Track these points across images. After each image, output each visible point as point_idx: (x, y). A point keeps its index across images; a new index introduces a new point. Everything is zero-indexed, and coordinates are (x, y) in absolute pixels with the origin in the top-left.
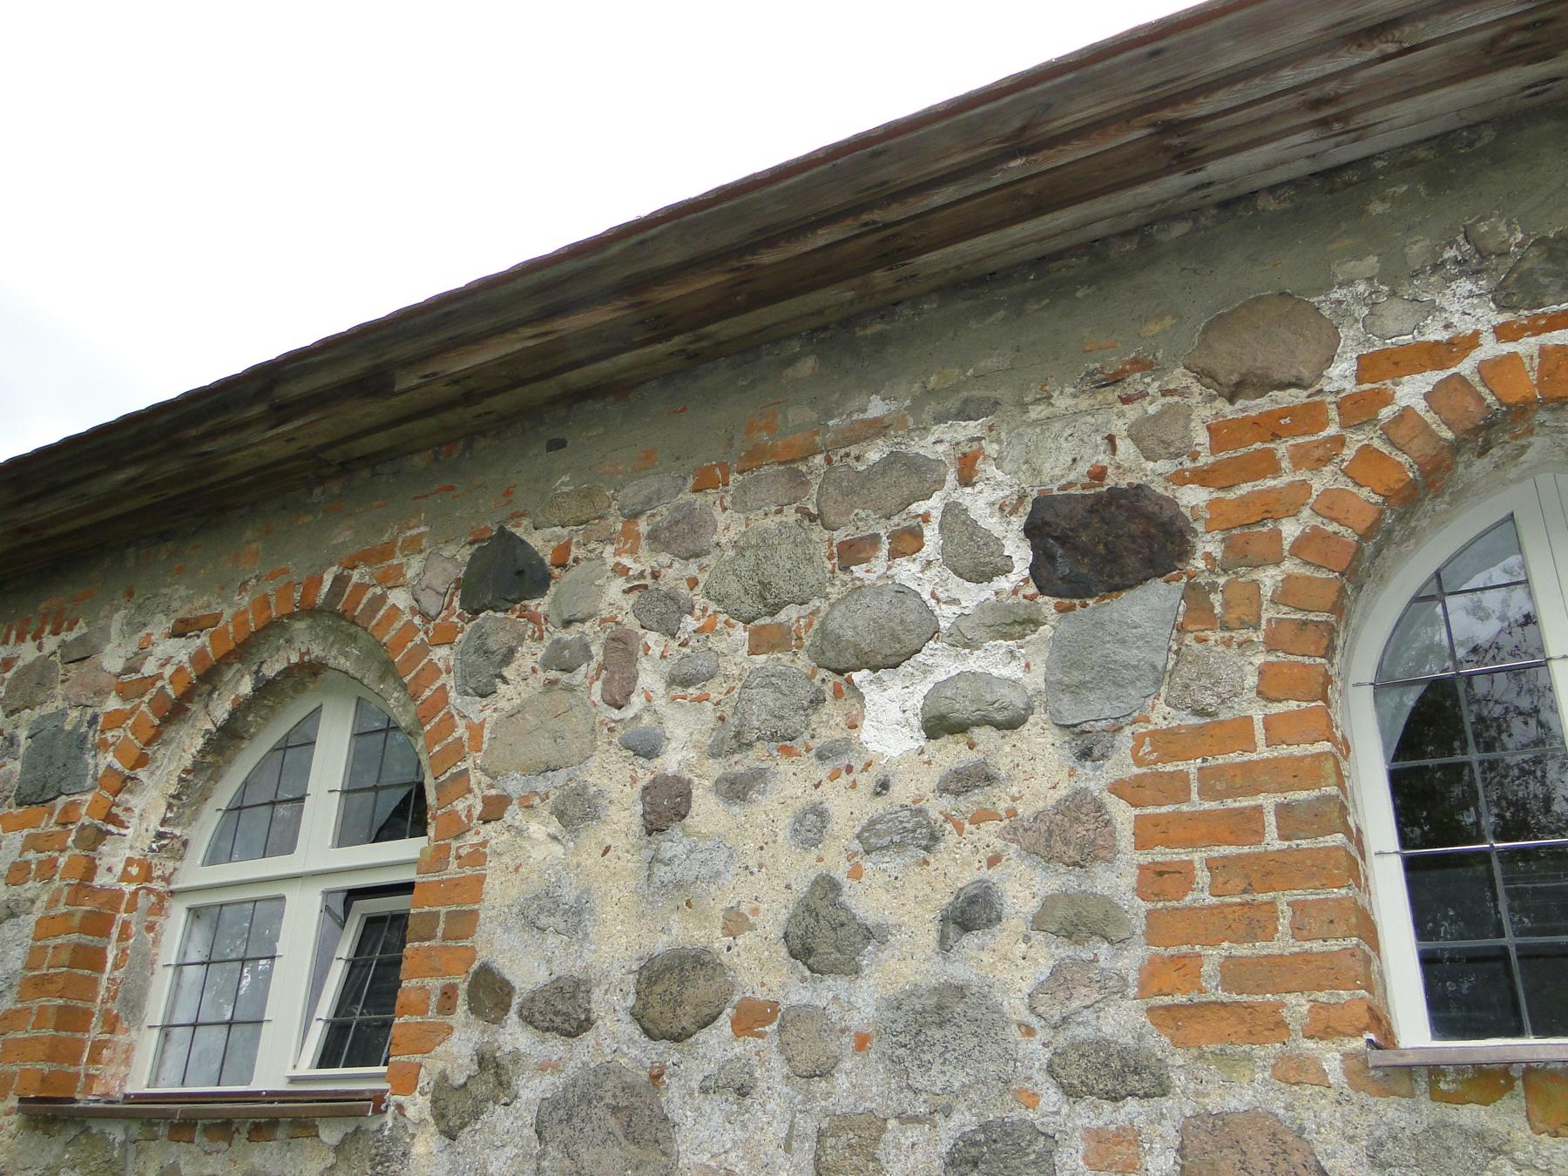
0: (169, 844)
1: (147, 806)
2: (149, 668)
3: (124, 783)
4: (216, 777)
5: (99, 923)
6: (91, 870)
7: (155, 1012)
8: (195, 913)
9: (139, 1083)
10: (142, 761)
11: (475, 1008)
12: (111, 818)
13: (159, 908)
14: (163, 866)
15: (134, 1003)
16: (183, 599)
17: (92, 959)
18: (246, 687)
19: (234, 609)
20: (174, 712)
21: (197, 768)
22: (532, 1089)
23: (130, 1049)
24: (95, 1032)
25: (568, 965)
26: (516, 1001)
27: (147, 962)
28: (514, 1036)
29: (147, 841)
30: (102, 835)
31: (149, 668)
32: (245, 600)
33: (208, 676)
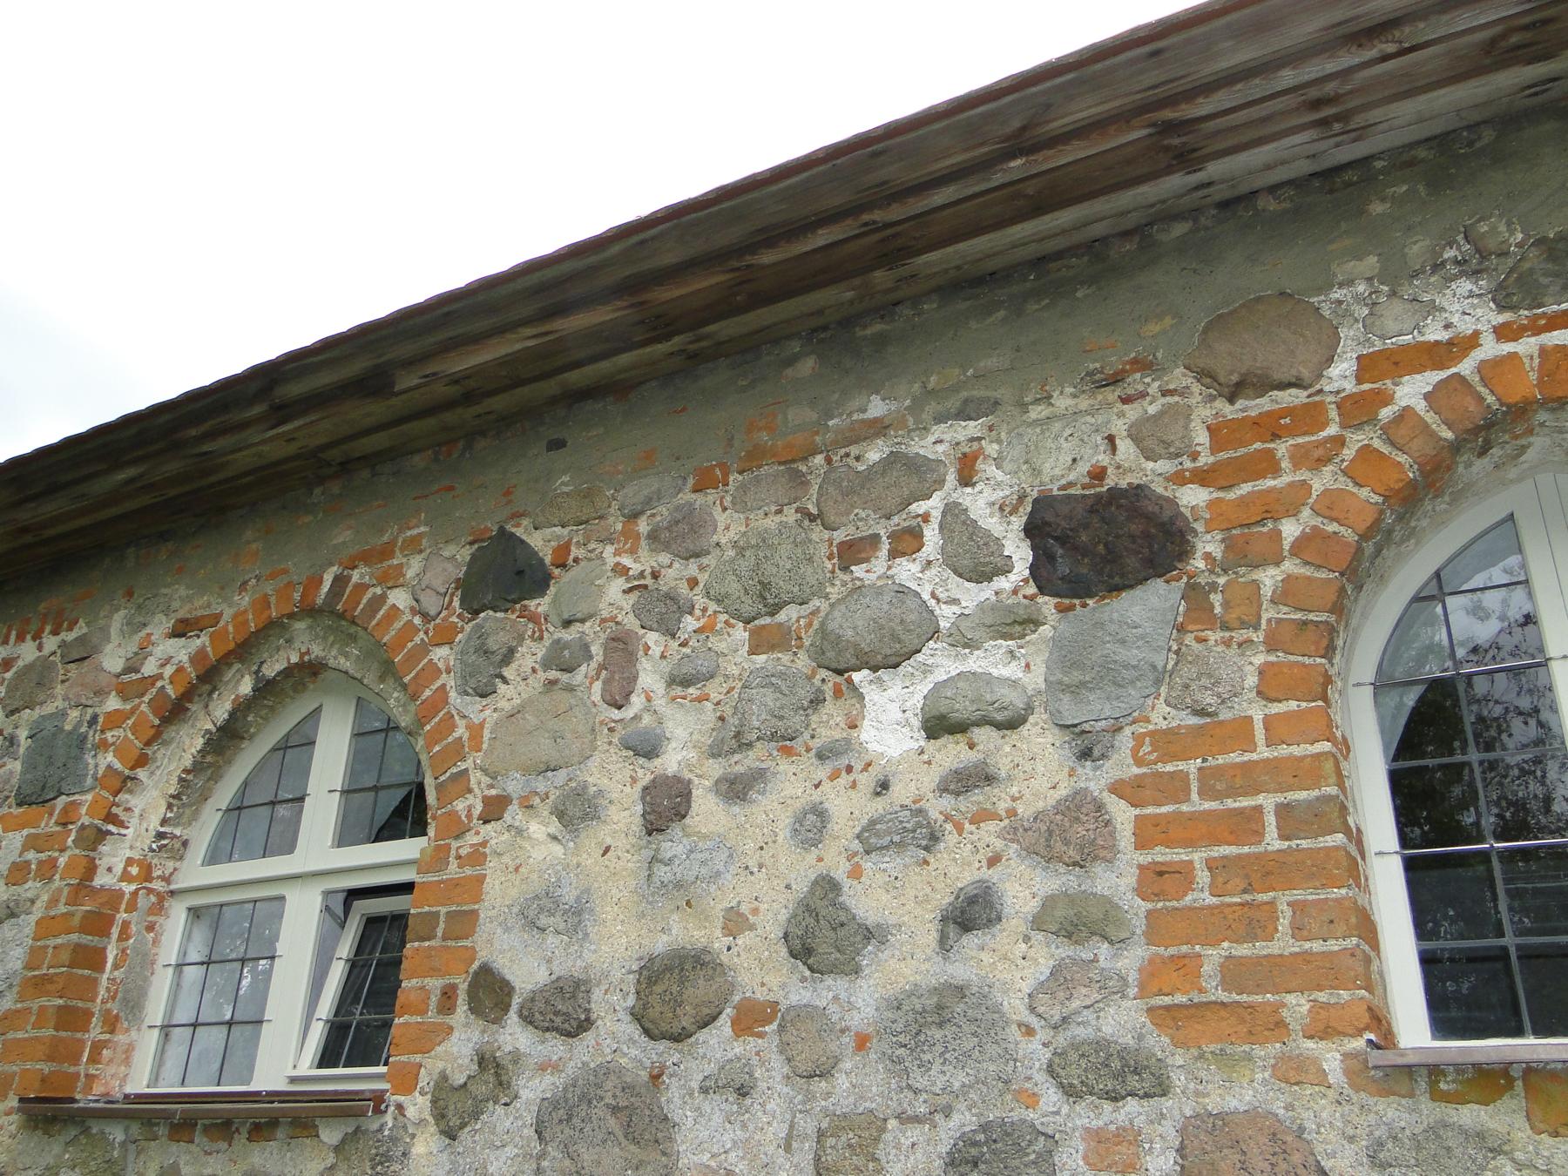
0: (169, 844)
1: (147, 806)
2: (149, 668)
3: (124, 783)
4: (216, 777)
5: (99, 923)
6: (91, 870)
7: (155, 1012)
8: (195, 913)
9: (139, 1083)
10: (142, 761)
11: (475, 1008)
12: (111, 818)
13: (159, 908)
14: (163, 866)
15: (134, 1003)
16: (183, 599)
17: (92, 959)
18: (246, 687)
19: (234, 609)
20: (174, 712)
21: (197, 768)
22: (532, 1089)
23: (130, 1049)
24: (95, 1032)
25: (568, 965)
26: (516, 1001)
27: (147, 962)
28: (514, 1036)
29: (147, 841)
30: (102, 835)
31: (149, 668)
32: (245, 600)
33: (208, 676)
